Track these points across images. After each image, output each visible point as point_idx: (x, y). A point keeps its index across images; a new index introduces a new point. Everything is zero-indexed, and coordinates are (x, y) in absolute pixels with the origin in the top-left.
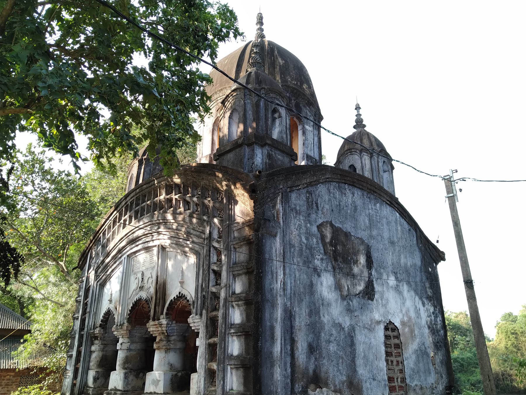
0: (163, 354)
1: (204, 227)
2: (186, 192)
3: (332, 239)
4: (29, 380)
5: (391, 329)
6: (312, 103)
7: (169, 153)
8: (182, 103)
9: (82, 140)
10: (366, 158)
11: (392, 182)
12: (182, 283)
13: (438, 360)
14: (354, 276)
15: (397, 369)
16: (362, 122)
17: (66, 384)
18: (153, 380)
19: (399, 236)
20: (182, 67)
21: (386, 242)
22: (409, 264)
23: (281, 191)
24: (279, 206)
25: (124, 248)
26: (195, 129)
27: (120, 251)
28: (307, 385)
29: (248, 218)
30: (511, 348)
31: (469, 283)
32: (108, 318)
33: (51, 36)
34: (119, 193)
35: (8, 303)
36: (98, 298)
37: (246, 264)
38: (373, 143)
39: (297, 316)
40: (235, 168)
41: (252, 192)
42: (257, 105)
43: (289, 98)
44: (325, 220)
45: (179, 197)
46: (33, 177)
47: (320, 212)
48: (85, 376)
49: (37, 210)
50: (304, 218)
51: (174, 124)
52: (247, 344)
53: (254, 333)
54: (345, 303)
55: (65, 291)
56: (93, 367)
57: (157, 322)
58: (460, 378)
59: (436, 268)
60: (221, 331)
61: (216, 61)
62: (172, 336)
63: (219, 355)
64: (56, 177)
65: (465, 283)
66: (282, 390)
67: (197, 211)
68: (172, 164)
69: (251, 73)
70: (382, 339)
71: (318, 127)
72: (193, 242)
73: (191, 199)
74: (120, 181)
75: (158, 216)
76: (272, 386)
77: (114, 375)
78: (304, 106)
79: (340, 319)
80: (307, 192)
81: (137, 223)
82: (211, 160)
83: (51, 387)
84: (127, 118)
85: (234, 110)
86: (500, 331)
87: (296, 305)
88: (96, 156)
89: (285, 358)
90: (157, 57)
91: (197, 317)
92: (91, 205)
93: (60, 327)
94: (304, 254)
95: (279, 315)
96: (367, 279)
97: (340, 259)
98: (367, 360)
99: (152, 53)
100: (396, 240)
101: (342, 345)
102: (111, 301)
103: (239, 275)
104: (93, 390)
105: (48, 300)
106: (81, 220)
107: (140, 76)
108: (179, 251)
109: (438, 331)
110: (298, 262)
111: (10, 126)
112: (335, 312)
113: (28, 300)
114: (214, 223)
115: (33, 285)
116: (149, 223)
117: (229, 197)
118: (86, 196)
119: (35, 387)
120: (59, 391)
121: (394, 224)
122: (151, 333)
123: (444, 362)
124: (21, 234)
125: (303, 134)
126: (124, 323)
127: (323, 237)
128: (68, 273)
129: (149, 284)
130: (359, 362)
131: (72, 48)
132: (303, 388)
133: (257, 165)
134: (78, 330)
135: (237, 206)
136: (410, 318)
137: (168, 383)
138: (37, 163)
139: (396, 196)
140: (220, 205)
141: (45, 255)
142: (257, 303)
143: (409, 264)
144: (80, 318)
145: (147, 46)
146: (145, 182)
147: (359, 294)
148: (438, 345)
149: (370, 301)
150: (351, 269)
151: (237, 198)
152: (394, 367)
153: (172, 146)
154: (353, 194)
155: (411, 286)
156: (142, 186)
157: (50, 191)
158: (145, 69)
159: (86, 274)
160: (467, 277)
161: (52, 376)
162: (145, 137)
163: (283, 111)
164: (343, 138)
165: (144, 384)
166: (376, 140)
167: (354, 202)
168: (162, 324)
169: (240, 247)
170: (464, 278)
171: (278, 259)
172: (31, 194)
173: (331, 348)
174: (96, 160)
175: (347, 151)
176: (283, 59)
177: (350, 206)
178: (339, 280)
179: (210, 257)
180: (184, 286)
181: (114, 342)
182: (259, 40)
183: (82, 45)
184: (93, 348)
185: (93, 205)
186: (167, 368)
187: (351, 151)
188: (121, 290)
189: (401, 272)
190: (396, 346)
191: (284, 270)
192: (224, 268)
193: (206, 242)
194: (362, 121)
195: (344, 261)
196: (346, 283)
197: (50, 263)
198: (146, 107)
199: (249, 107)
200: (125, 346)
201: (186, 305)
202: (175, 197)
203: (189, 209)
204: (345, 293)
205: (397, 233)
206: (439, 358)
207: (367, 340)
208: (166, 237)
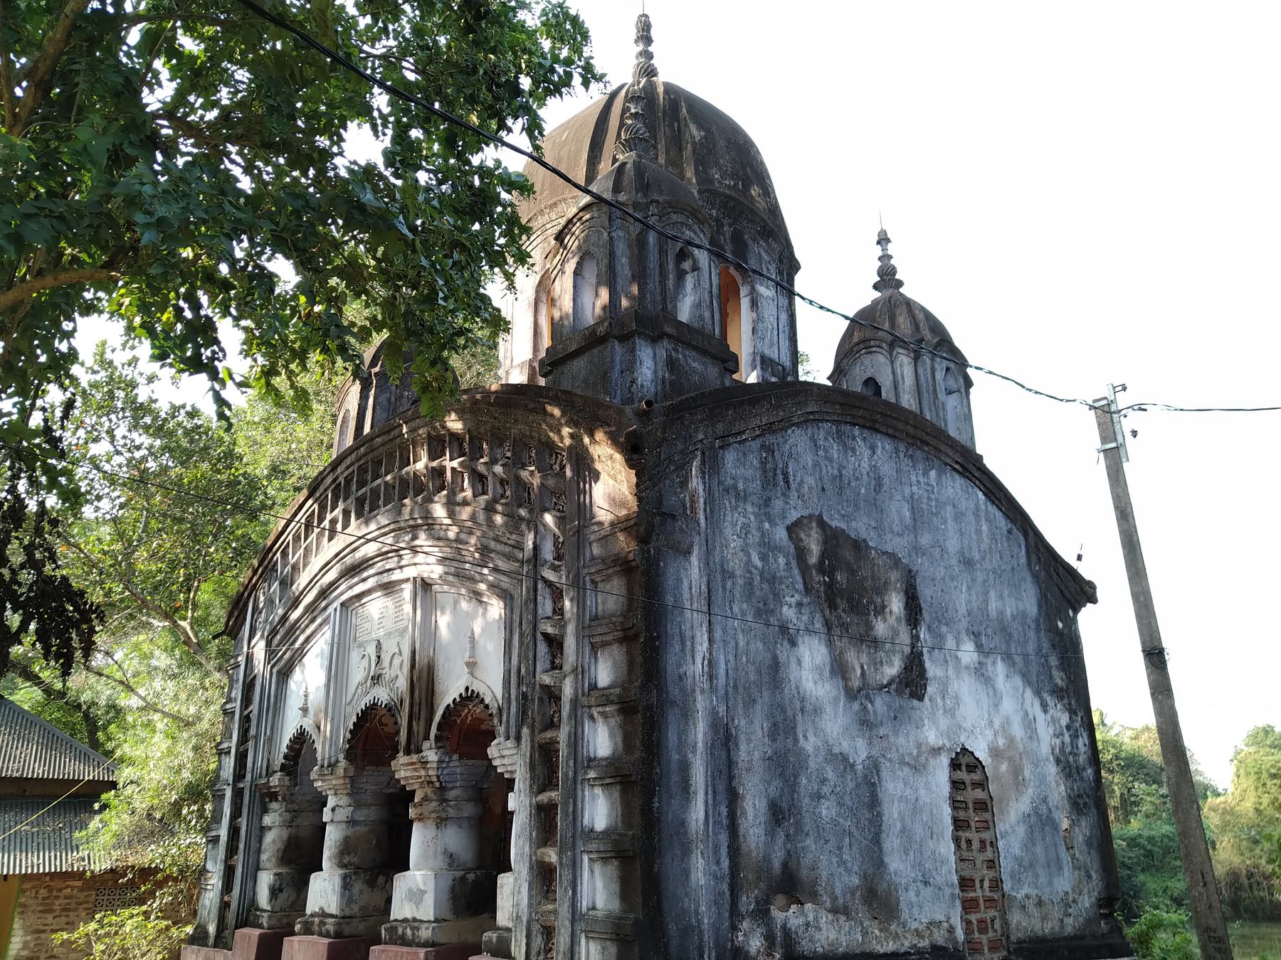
0: (431, 831)
2: (476, 454)
3: (823, 556)
4: (117, 897)
5: (967, 766)
7: (433, 363)
8: (464, 248)
11: (968, 417)
12: (472, 665)
13: (1081, 838)
14: (875, 643)
15: (980, 858)
16: (894, 274)
17: (207, 903)
18: (410, 890)
19: (984, 546)
20: (461, 157)
21: (954, 562)
22: (1009, 613)
25: (333, 585)
26: (495, 304)
27: (323, 594)
29: (624, 512)
30: (1270, 811)
31: (1155, 656)
32: (300, 750)
33: (152, 91)
35: (58, 720)
36: (275, 704)
38: (921, 325)
39: (742, 738)
40: (590, 394)
41: (633, 450)
42: (641, 243)
43: (717, 220)
44: (806, 513)
45: (461, 464)
46: (110, 421)
47: (794, 494)
48: (250, 884)
49: (122, 500)
50: (756, 510)
51: (445, 299)
52: (626, 805)
53: (643, 776)
54: (856, 706)
56: (268, 865)
57: (414, 758)
58: (1144, 884)
59: (1074, 621)
60: (566, 775)
62: (452, 788)
63: (562, 829)
64: (166, 419)
65: (1146, 656)
66: (710, 908)
67: (502, 496)
68: (443, 389)
69: (624, 164)
70: (945, 789)
71: (789, 292)
72: (496, 570)
73: (488, 470)
74: (317, 425)
76: (686, 900)
77: (318, 881)
78: (754, 240)
79: (845, 744)
80: (762, 446)
81: (363, 526)
82: (532, 376)
84: (334, 281)
85: (585, 256)
86: (1242, 771)
87: (741, 711)
88: (262, 371)
89: (715, 834)
90: (401, 136)
91: (510, 743)
92: (248, 484)
94: (758, 593)
95: (700, 736)
96: (907, 650)
97: (842, 604)
100: (977, 556)
101: (850, 804)
102: (305, 710)
103: (605, 644)
104: (270, 917)
105: (156, 711)
106: (225, 520)
107: (365, 188)
108: (463, 591)
109: (1079, 770)
110: (743, 613)
111: (63, 306)
112: (831, 728)
113: (108, 713)
114: (545, 525)
115: (118, 675)
116: (392, 527)
117: (578, 465)
122: (402, 783)
123: (1095, 844)
124: (87, 556)
125: (752, 307)
126: (337, 761)
128: (201, 646)
130: (891, 842)
131: (202, 117)
132: (757, 903)
133: (642, 386)
136: (1011, 740)
137: (445, 896)
138: (119, 388)
140: (558, 483)
142: (649, 708)
143: (1009, 613)
144: (233, 751)
145: (379, 110)
146: (378, 431)
147: (889, 684)
148: (1080, 801)
149: (915, 702)
150: (870, 627)
151: (598, 466)
152: (975, 853)
153: (443, 347)
154: (873, 449)
156: (373, 439)
157: (151, 454)
158: (374, 167)
159: (245, 649)
160: (1151, 641)
161: (170, 888)
162: (377, 325)
163: (702, 257)
164: (847, 318)
165: (389, 901)
166: (929, 316)
167: (874, 468)
168: (427, 762)
169: (607, 579)
170: (1143, 643)
172: (108, 461)
173: (824, 812)
174: (263, 381)
175: (858, 344)
176: (700, 127)
177: (865, 477)
178: (841, 653)
179: (536, 604)
180: (478, 673)
181: (315, 807)
182: (643, 81)
183: (226, 114)
184: (267, 820)
185: (253, 484)
186: (440, 862)
187: (867, 344)
189: (989, 631)
190: (978, 806)
191: (710, 631)
192: (570, 629)
193: (525, 569)
194: (893, 271)
195: (851, 609)
196: (856, 659)
197: (155, 622)
198: (379, 254)
199: (621, 248)
200: (342, 814)
202: (451, 464)
203: (484, 493)
204: (856, 683)
205: (980, 540)
206: (1083, 831)
207: (908, 792)
208: (432, 559)
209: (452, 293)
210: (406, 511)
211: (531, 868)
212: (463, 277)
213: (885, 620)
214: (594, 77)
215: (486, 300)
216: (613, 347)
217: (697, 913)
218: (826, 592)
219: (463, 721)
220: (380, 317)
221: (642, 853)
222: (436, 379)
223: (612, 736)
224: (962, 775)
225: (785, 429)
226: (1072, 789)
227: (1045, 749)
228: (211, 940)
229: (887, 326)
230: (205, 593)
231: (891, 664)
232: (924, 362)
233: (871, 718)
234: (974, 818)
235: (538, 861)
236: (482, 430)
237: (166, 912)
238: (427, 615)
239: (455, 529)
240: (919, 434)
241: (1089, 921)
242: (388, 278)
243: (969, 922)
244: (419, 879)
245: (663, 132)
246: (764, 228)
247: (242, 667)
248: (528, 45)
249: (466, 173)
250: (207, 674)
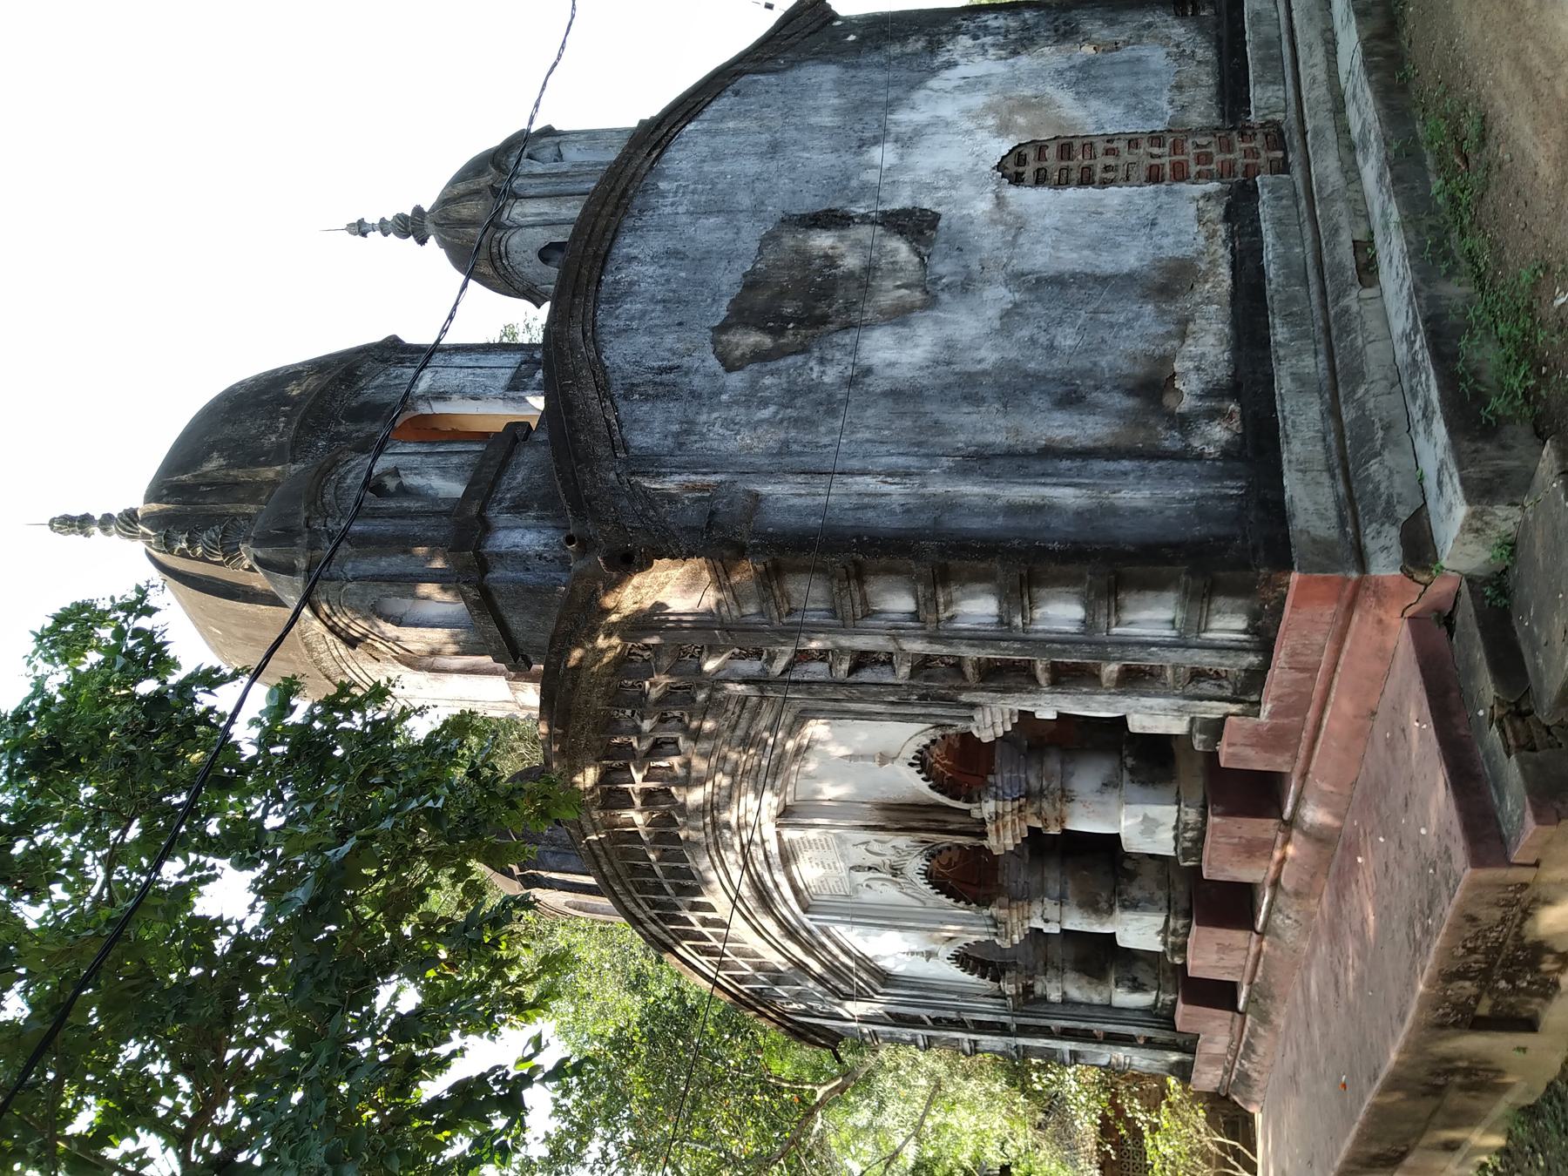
0: (1076, 808)
1: (729, 698)
2: (627, 752)
5: (1018, 165)
7: (513, 806)
8: (369, 772)
9: (477, 1055)
10: (520, 211)
11: (592, 136)
12: (884, 759)
13: (1105, 32)
14: (870, 269)
15: (1126, 156)
16: (405, 217)
17: (1145, 1063)
18: (1142, 833)
19: (754, 126)
21: (773, 165)
24: (671, 484)
25: (782, 923)
27: (791, 934)
28: (1165, 415)
29: (706, 575)
32: (975, 959)
33: (150, 1161)
34: (619, 939)
36: (920, 989)
37: (836, 581)
38: (473, 187)
39: (980, 438)
41: (629, 562)
42: (362, 541)
43: (331, 440)
45: (639, 770)
47: (686, 362)
50: (705, 410)
51: (435, 798)
53: (1024, 560)
55: (899, 1079)
56: (1106, 995)
57: (990, 827)
59: (847, 20)
60: (1017, 651)
64: (571, 1122)
67: (680, 720)
69: (257, 560)
70: (1044, 194)
71: (425, 355)
72: (772, 729)
73: (647, 737)
75: (694, 829)
76: (1168, 513)
80: (626, 398)
81: (712, 887)
82: (532, 679)
87: (948, 439)
88: (517, 1013)
91: (978, 716)
92: (653, 1020)
93: (997, 1088)
94: (807, 412)
95: (976, 490)
97: (822, 308)
99: (202, 859)
100: (766, 137)
101: (1060, 311)
102: (929, 955)
103: (865, 601)
105: (922, 1123)
108: (795, 768)
109: (1026, 28)
110: (831, 431)
112: (970, 329)
114: (718, 670)
116: (713, 853)
117: (644, 629)
118: (626, 1033)
120: (1163, 1080)
121: (718, 141)
123: (1112, 15)
125: (445, 399)
126: (991, 917)
128: (847, 1073)
129: (887, 849)
130: (1106, 263)
131: (186, 1096)
132: (1171, 428)
133: (545, 545)
134: (1005, 1039)
135: (669, 603)
136: (990, 109)
137: (1150, 792)
139: (634, 124)
141: (795, 1141)
142: (942, 551)
143: (836, 101)
144: (973, 1037)
145: (180, 875)
147: (919, 254)
149: (942, 224)
150: (850, 275)
151: (648, 604)
152: (1120, 162)
154: (631, 259)
155: (898, 99)
156: (604, 876)
158: (257, 881)
159: (854, 1025)
162: (462, 873)
163: (384, 463)
164: (465, 286)
169: (786, 596)
171: (821, 491)
173: (1069, 342)
174: (529, 1012)
175: (496, 269)
176: (206, 457)
177: (666, 271)
181: (1041, 941)
182: (142, 528)
184: (1055, 996)
185: (654, 1013)
186: (1112, 797)
187: (496, 257)
189: (858, 127)
191: (852, 473)
192: (845, 642)
193: (771, 694)
194: (401, 218)
195: (827, 297)
196: (889, 294)
197: (818, 1126)
199: (367, 566)
200: (1052, 910)
201: (944, 746)
202: (638, 781)
203: (675, 742)
204: (917, 296)
207: (1047, 239)
209: (424, 786)
210: (694, 835)
211: (1124, 694)
212: (405, 772)
213: (842, 256)
214: (140, 601)
215: (430, 742)
216: (496, 580)
217: (1182, 501)
218: (811, 327)
219: (949, 769)
221: (1110, 563)
222: (533, 802)
223: (973, 596)
224: (1029, 171)
225: (604, 369)
226: (1048, 38)
227: (1000, 68)
228: (1188, 1058)
230: (782, 1068)
231: (895, 251)
232: (520, 186)
233: (959, 279)
235: (1117, 686)
238: (821, 811)
239: (719, 777)
240: (613, 200)
241: (1201, 30)
242: (404, 860)
243: (1199, 175)
244: (1130, 822)
245: (214, 506)
246: (342, 381)
247: (876, 1028)
248: (95, 685)
249: (268, 764)
250: (881, 1064)
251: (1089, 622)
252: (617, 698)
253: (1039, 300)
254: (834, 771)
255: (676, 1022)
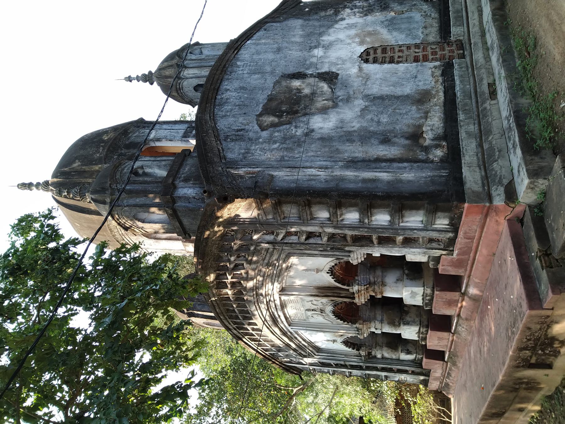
2: (225, 268)
6: (124, 130)
7: (184, 288)
8: (132, 276)
9: (171, 378)
10: (187, 73)
11: (213, 45)
12: (318, 271)
13: (399, 7)
14: (313, 94)
15: (406, 53)
17: (412, 380)
18: (411, 297)
19: (272, 42)
21: (278, 56)
23: (224, 169)
25: (281, 330)
27: (285, 334)
29: (254, 205)
32: (351, 343)
33: (53, 416)
36: (331, 353)
37: (301, 207)
38: (170, 64)
39: (353, 155)
41: (226, 200)
42: (130, 192)
43: (119, 156)
44: (255, 122)
45: (230, 275)
47: (247, 127)
48: (405, 363)
50: (254, 145)
51: (156, 285)
55: (323, 386)
56: (397, 355)
57: (356, 295)
59: (305, 3)
60: (366, 232)
61: (81, 239)
64: (205, 401)
67: (245, 257)
69: (92, 199)
71: (152, 125)
72: (278, 260)
73: (233, 263)
75: (249, 296)
76: (420, 182)
77: (405, 335)
80: (225, 140)
81: (256, 317)
82: (191, 242)
83: (414, 394)
87: (341, 156)
88: (186, 362)
89: (393, 169)
90: (77, 302)
91: (352, 255)
92: (235, 364)
93: (358, 389)
94: (290, 146)
95: (351, 174)
96: (317, 79)
97: (296, 108)
98: (397, 83)
99: (72, 307)
100: (276, 46)
101: (382, 109)
102: (334, 341)
103: (311, 214)
105: (331, 402)
108: (286, 274)
110: (299, 152)
112: (349, 115)
114: (258, 239)
116: (256, 304)
117: (231, 224)
119: (413, 409)
120: (418, 386)
121: (259, 47)
125: (160, 141)
126: (356, 327)
127: (273, 125)
130: (399, 91)
131: (67, 392)
133: (196, 194)
135: (241, 214)
136: (357, 35)
141: (286, 408)
143: (301, 33)
144: (350, 371)
145: (64, 313)
147: (331, 88)
149: (339, 77)
150: (306, 96)
151: (233, 215)
152: (404, 55)
154: (227, 90)
162: (166, 312)
163: (138, 164)
164: (167, 100)
165: (414, 306)
166: (166, 60)
167: (236, 90)
169: (283, 212)
173: (385, 120)
174: (190, 362)
175: (178, 94)
176: (74, 162)
177: (240, 94)
178: (317, 109)
180: (321, 268)
182: (51, 187)
184: (379, 356)
185: (235, 362)
186: (400, 284)
188: (324, 332)
189: (309, 42)
191: (307, 168)
192: (304, 229)
194: (144, 75)
196: (320, 103)
197: (294, 403)
199: (132, 201)
200: (378, 325)
201: (339, 266)
202: (229, 279)
203: (243, 265)
204: (331, 103)
207: (377, 82)
209: (152, 281)
210: (249, 298)
211: (404, 247)
213: (303, 89)
214: (49, 214)
215: (154, 265)
216: (178, 206)
217: (426, 177)
218: (290, 115)
219: (341, 274)
220: (163, 311)
221: (400, 200)
222: (191, 286)
223: (350, 212)
226: (378, 9)
227: (361, 20)
228: (427, 378)
229: (171, 80)
231: (323, 87)
234: (389, 54)
236: (215, 265)
237: (414, 395)
239: (258, 277)
240: (220, 68)
241: (433, 7)
242: (145, 307)
243: (432, 59)
244: (406, 294)
245: (76, 179)
247: (315, 367)
249: (96, 273)
251: (392, 221)
252: (222, 249)
253: (374, 105)
254: (300, 275)
255: (243, 365)
